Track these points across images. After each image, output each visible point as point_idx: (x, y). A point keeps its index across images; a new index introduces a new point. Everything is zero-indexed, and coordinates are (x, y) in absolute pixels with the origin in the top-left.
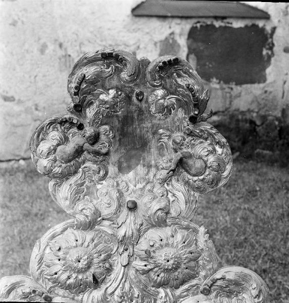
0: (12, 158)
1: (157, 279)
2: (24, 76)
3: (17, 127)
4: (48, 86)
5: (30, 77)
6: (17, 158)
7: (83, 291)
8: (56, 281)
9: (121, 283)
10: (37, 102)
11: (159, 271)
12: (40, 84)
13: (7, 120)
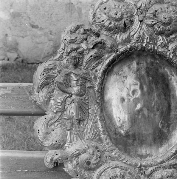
0: (35, 62)
1: (158, 29)
2: (44, 13)
3: (39, 43)
4: (58, 21)
5: (48, 14)
6: (38, 62)
7: (117, 33)
8: (103, 26)
9: (138, 30)
10: (51, 30)
11: (160, 24)
12: (54, 19)
13: (33, 39)
